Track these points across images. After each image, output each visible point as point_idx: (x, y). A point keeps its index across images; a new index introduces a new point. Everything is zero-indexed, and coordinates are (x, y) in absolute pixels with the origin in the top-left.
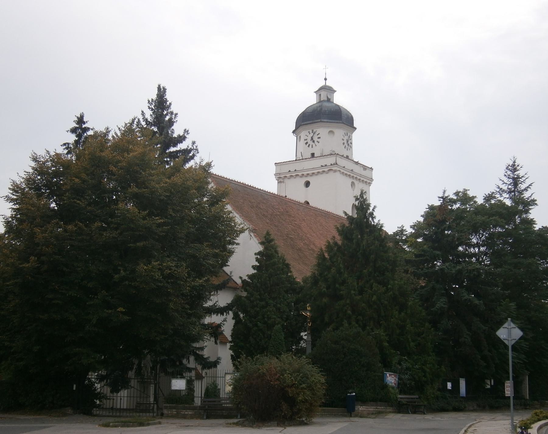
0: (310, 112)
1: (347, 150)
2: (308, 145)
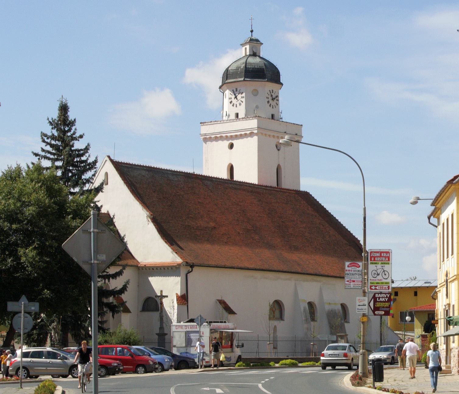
0: (234, 70)
1: (273, 108)
2: (232, 104)
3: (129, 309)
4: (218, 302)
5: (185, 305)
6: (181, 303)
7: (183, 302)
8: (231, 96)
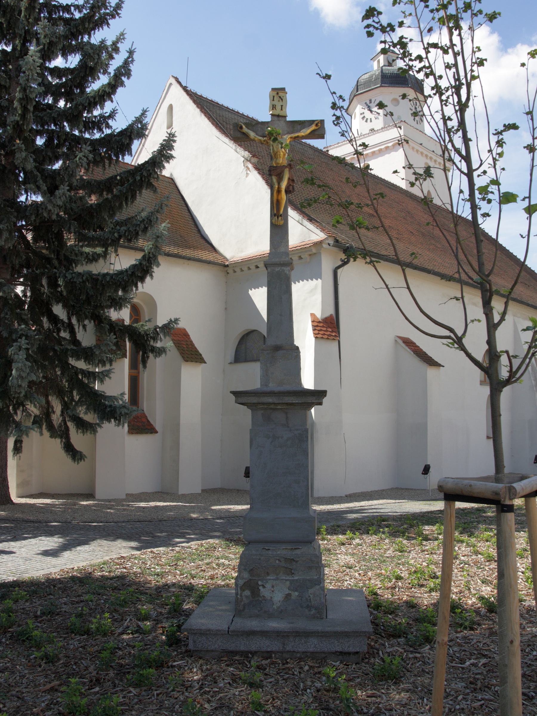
3: (201, 355)
4: (400, 342)
5: (334, 339)
6: (324, 334)
7: (329, 333)
8: (363, 111)
